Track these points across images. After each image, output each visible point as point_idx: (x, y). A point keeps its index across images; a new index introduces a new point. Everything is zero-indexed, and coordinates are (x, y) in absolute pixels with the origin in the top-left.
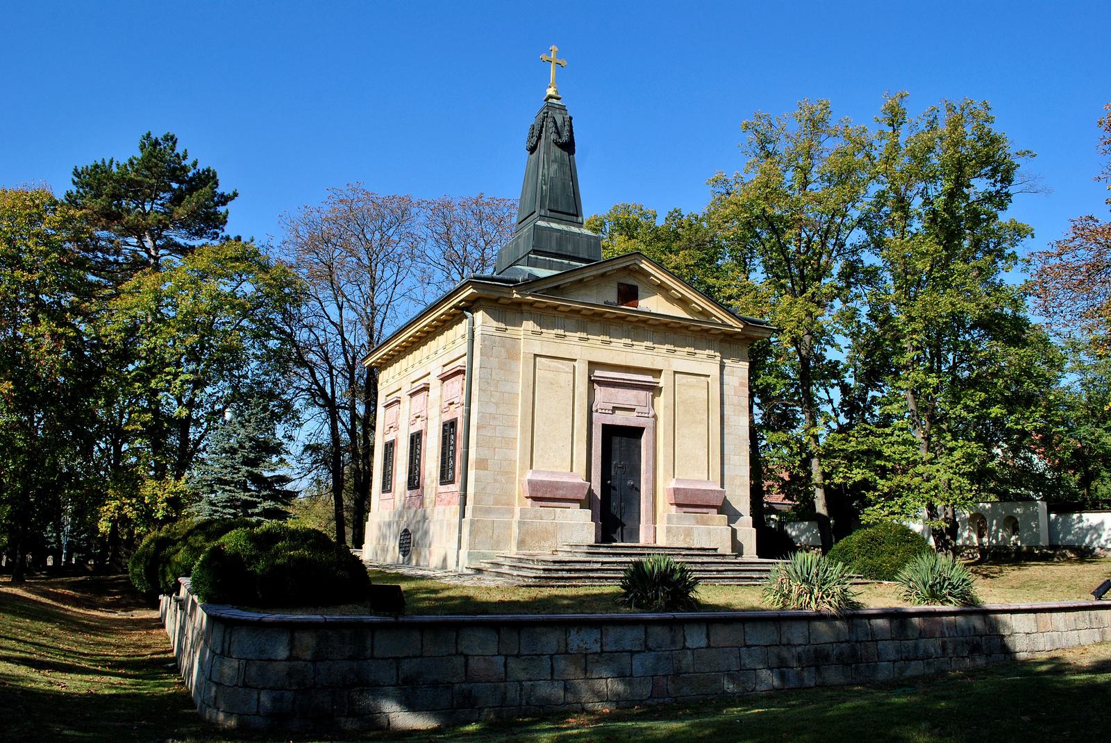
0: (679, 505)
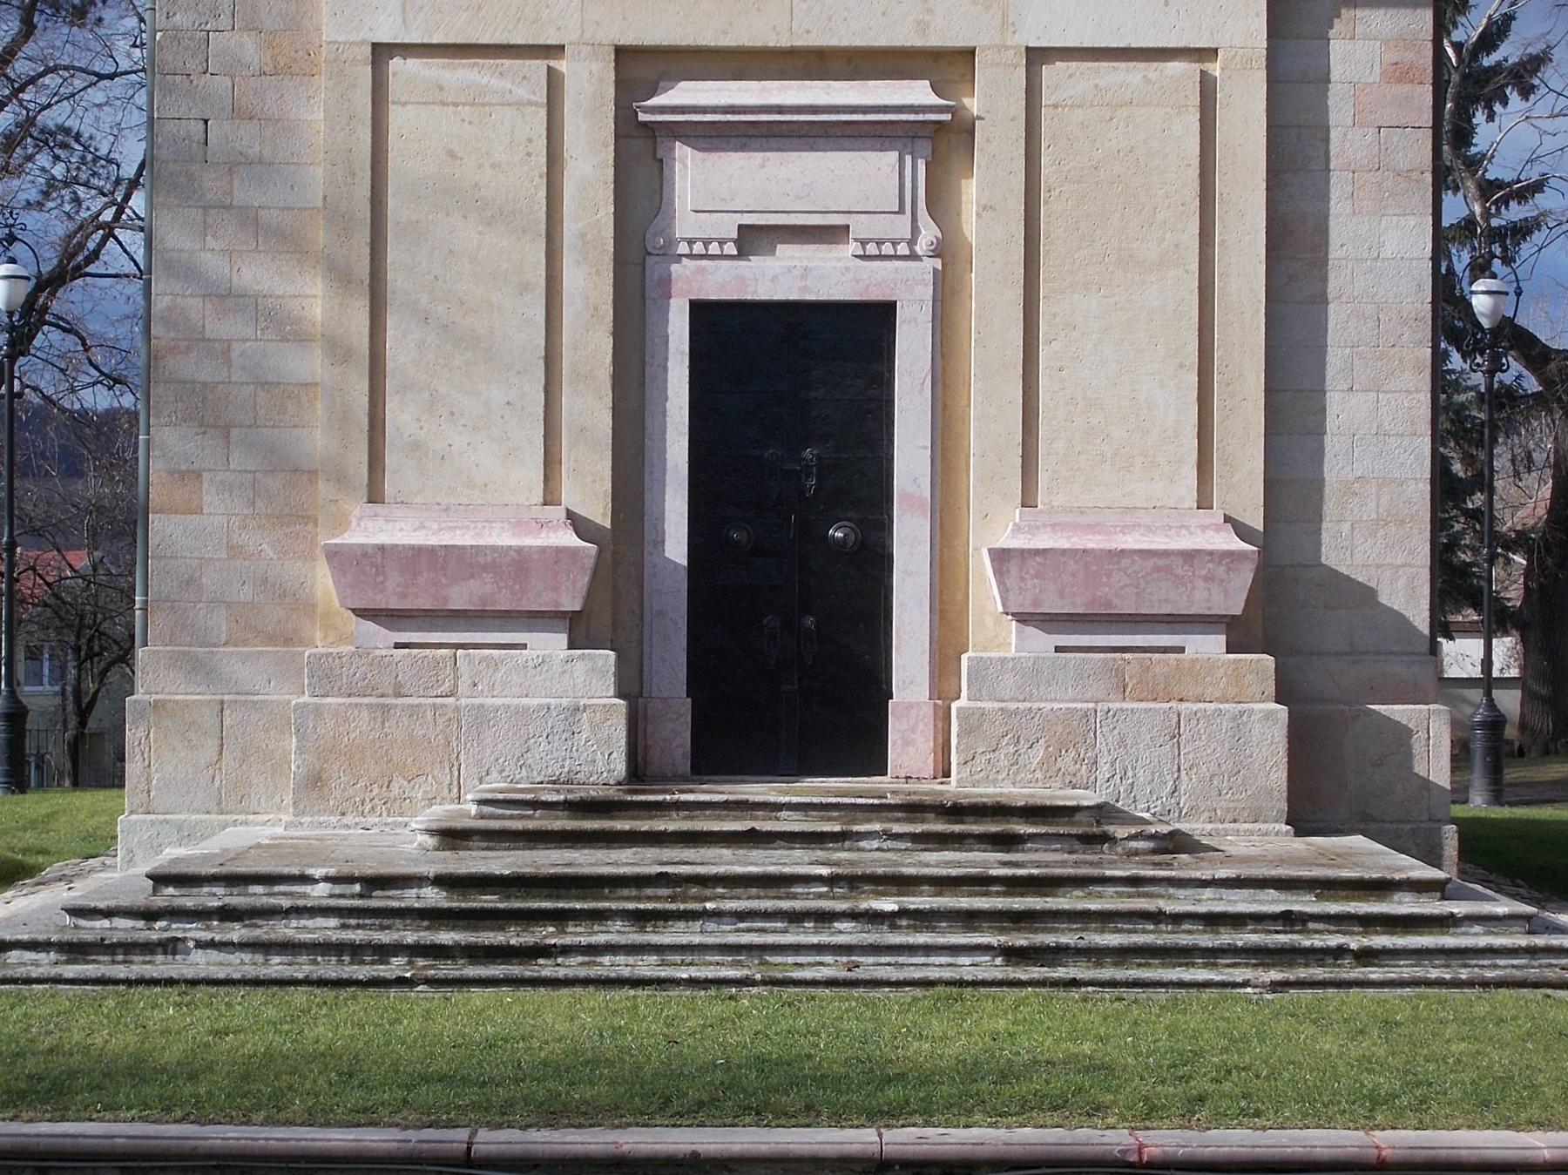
0: (1023, 618)
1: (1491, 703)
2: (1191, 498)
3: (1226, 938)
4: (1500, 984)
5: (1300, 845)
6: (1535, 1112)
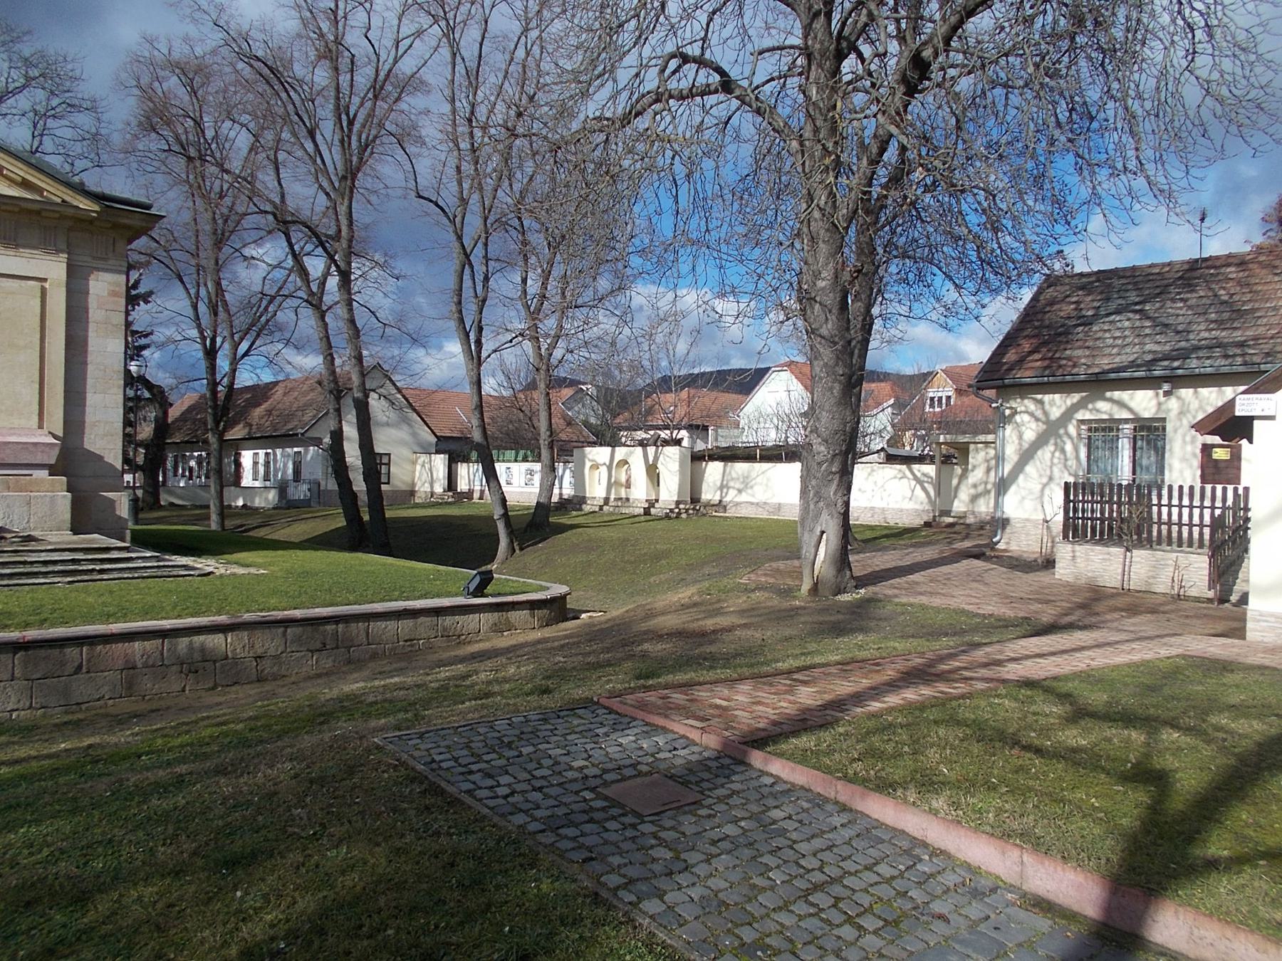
1: (135, 494)
2: (35, 425)
3: (50, 568)
4: (148, 577)
5: (76, 537)
6: (164, 614)
